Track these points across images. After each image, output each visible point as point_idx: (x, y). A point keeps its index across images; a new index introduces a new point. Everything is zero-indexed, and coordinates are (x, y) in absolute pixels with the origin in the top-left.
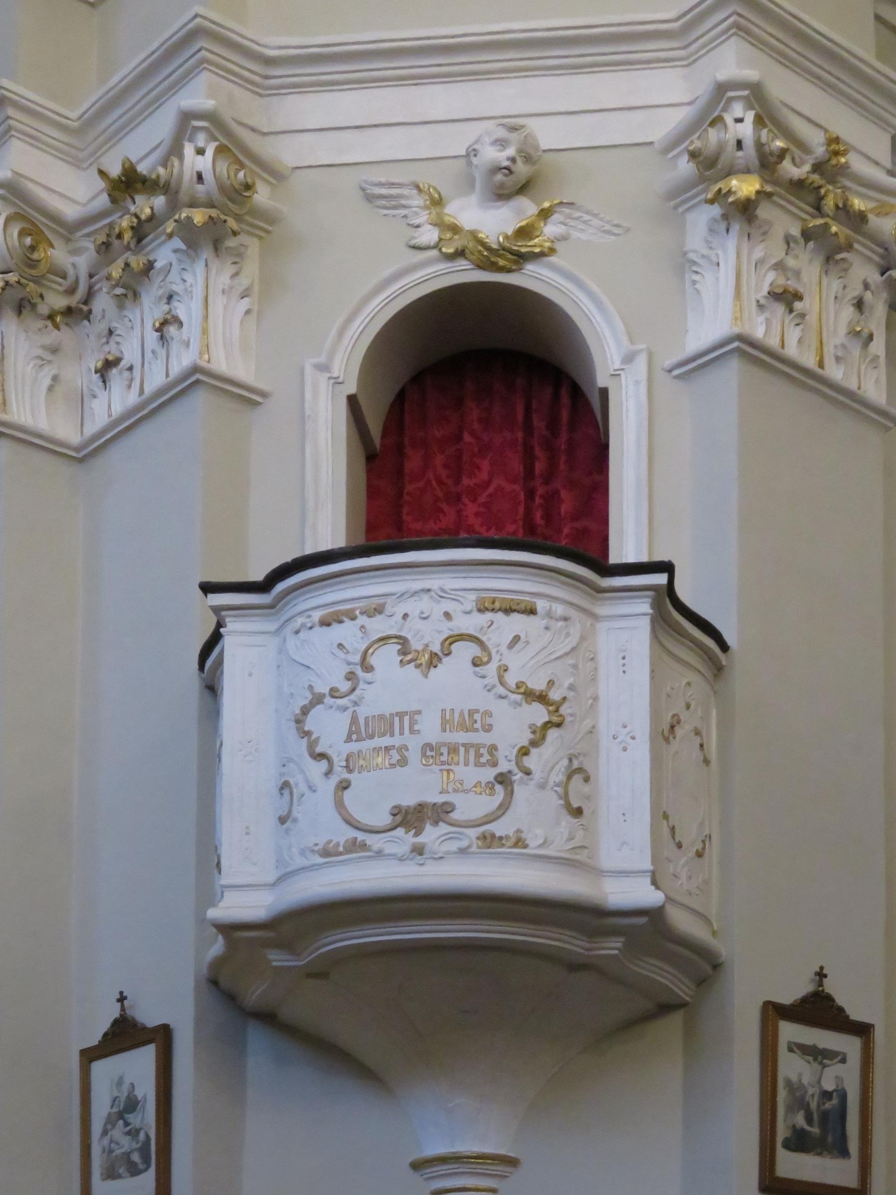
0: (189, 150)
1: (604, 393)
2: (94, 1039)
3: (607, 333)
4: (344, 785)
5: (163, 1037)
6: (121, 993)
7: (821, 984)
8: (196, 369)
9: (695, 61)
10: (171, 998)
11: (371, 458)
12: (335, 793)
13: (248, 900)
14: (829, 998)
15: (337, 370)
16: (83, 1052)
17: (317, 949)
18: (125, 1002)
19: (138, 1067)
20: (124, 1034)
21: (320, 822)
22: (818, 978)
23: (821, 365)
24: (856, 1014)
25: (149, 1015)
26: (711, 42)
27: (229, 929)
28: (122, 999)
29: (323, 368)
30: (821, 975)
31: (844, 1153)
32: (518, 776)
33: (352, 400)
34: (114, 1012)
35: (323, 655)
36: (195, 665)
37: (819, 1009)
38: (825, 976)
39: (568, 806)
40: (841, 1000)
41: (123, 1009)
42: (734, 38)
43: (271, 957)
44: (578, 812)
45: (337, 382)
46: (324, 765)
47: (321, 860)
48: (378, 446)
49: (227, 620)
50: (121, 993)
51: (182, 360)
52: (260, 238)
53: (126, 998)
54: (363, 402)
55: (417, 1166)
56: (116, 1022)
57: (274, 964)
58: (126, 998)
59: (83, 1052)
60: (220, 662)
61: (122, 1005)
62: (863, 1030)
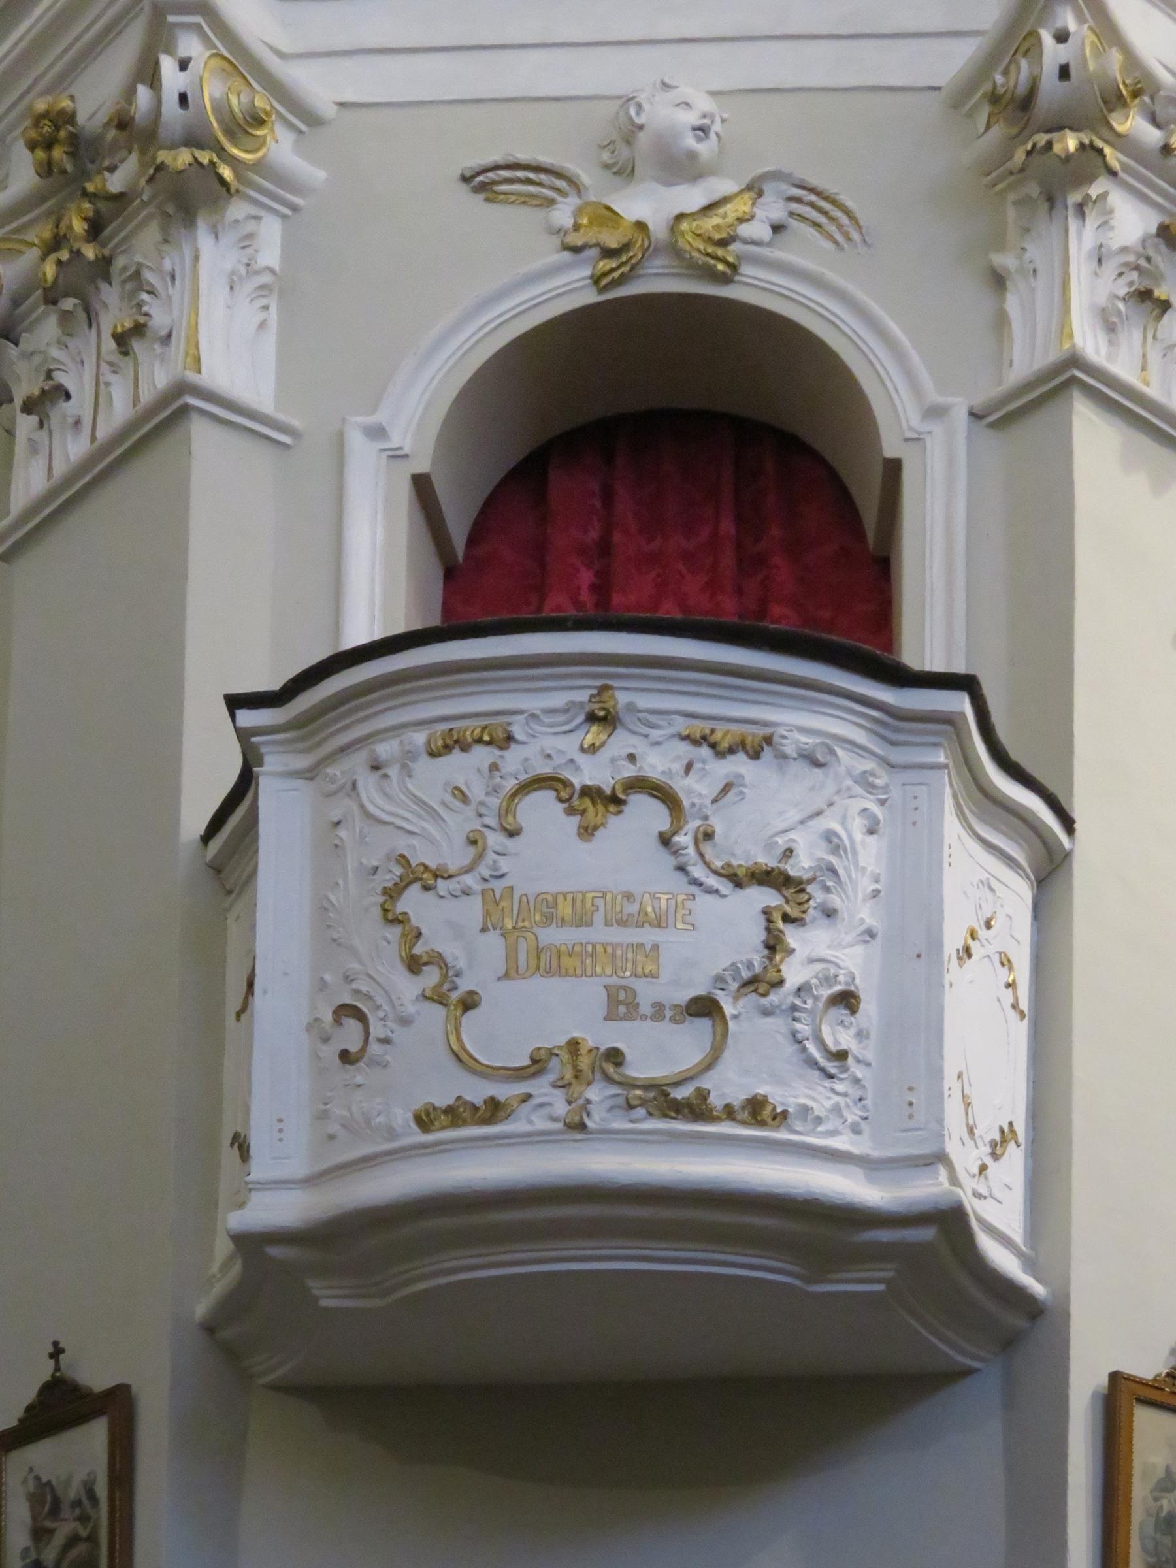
0: (168, 65)
1: (893, 468)
5: (117, 1404)
6: (56, 1344)
8: (181, 388)
9: (812, 190)
11: (450, 573)
12: (1003, 1154)
13: (277, 1199)
15: (399, 438)
17: (406, 1283)
18: (62, 1356)
19: (83, 1451)
20: (61, 1405)
27: (250, 1244)
28: (57, 1352)
29: (377, 432)
33: (422, 485)
34: (44, 1371)
39: (361, 1017)
41: (57, 1368)
43: (316, 1292)
45: (397, 456)
48: (460, 559)
49: (263, 750)
50: (56, 1344)
51: (157, 375)
52: (284, 217)
53: (62, 1351)
54: (442, 489)
57: (324, 1303)
58: (62, 1351)
60: (252, 822)
61: (57, 1362)
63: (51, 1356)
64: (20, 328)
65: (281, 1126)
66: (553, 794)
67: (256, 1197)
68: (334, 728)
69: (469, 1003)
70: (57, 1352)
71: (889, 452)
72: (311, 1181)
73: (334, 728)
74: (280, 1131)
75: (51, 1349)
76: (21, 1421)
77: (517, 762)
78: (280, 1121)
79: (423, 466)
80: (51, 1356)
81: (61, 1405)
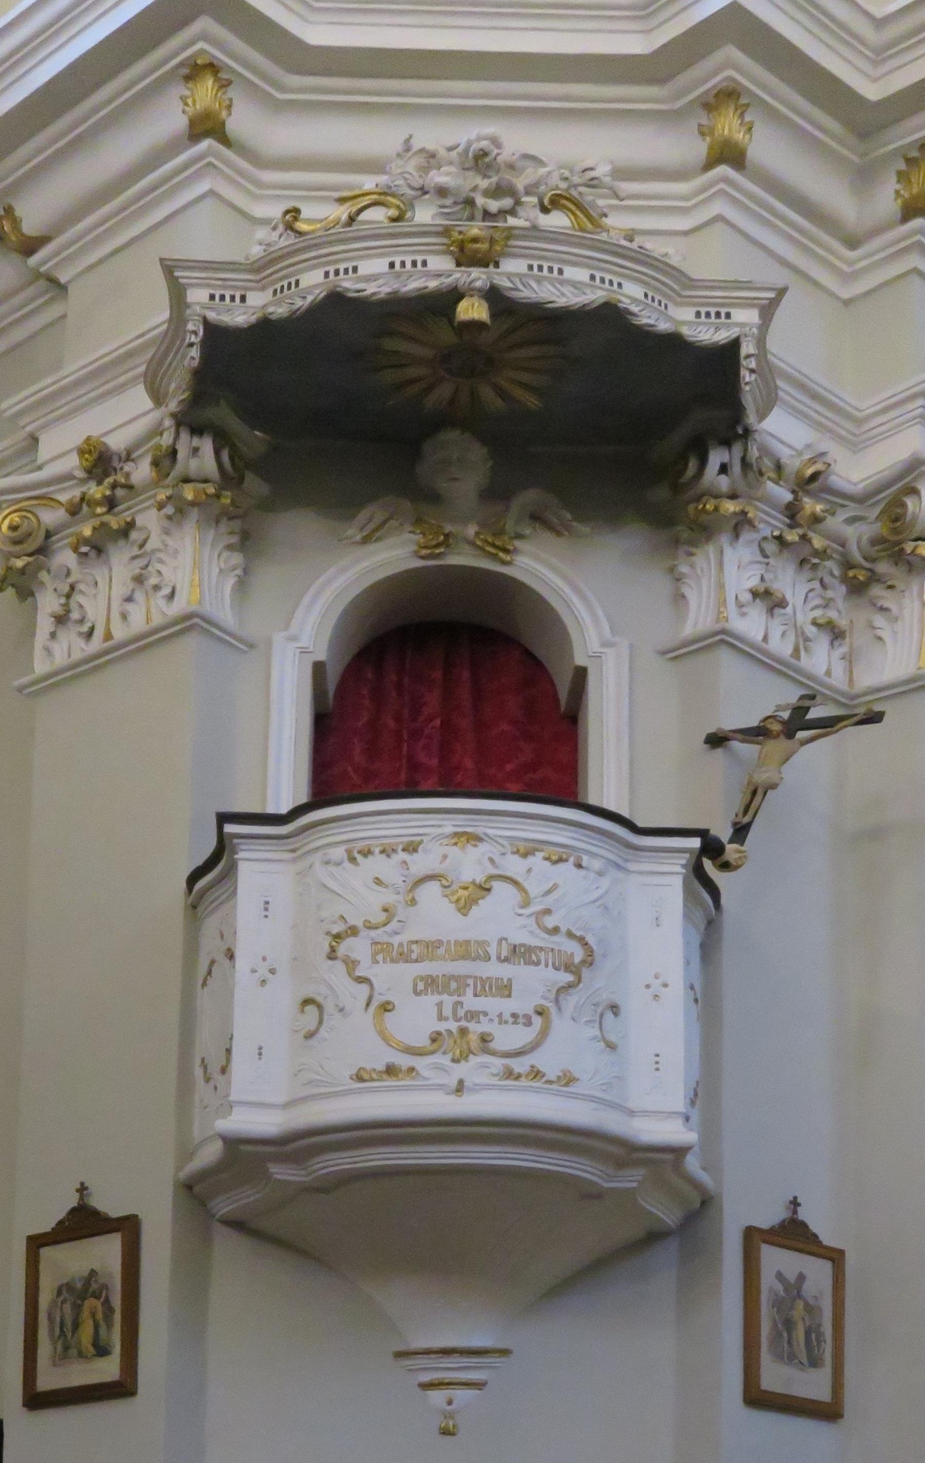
2: (46, 1225)
3: (575, 600)
4: (390, 1007)
5: (129, 1228)
6: (82, 1184)
7: (795, 1212)
10: (145, 1192)
14: (804, 1225)
16: (30, 1239)
19: (105, 1253)
20: (83, 1222)
21: (354, 1042)
22: (792, 1206)
23: (765, 639)
24: (827, 1239)
25: (109, 1204)
26: (899, 426)
30: (795, 1203)
31: (814, 1362)
32: (553, 1010)
34: (73, 1201)
35: (360, 890)
36: (184, 885)
37: (794, 1233)
38: (799, 1205)
40: (815, 1227)
41: (82, 1198)
42: (918, 427)
44: (611, 1046)
46: (364, 989)
47: (495, 1081)
50: (82, 1184)
55: (400, 1355)
56: (73, 1211)
59: (30, 1239)
62: (836, 1257)
63: (77, 1191)
64: (55, 546)
65: (657, 1059)
66: (439, 883)
67: (236, 1110)
68: (335, 831)
69: (386, 1007)
70: (82, 1189)
71: (580, 660)
72: (286, 1106)
73: (335, 831)
74: (657, 1063)
75: (78, 1186)
76: (53, 1229)
77: (421, 863)
78: (657, 1055)
79: (321, 656)
80: (77, 1191)
81: (83, 1222)
